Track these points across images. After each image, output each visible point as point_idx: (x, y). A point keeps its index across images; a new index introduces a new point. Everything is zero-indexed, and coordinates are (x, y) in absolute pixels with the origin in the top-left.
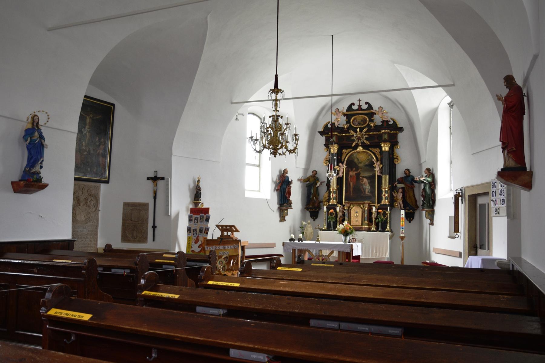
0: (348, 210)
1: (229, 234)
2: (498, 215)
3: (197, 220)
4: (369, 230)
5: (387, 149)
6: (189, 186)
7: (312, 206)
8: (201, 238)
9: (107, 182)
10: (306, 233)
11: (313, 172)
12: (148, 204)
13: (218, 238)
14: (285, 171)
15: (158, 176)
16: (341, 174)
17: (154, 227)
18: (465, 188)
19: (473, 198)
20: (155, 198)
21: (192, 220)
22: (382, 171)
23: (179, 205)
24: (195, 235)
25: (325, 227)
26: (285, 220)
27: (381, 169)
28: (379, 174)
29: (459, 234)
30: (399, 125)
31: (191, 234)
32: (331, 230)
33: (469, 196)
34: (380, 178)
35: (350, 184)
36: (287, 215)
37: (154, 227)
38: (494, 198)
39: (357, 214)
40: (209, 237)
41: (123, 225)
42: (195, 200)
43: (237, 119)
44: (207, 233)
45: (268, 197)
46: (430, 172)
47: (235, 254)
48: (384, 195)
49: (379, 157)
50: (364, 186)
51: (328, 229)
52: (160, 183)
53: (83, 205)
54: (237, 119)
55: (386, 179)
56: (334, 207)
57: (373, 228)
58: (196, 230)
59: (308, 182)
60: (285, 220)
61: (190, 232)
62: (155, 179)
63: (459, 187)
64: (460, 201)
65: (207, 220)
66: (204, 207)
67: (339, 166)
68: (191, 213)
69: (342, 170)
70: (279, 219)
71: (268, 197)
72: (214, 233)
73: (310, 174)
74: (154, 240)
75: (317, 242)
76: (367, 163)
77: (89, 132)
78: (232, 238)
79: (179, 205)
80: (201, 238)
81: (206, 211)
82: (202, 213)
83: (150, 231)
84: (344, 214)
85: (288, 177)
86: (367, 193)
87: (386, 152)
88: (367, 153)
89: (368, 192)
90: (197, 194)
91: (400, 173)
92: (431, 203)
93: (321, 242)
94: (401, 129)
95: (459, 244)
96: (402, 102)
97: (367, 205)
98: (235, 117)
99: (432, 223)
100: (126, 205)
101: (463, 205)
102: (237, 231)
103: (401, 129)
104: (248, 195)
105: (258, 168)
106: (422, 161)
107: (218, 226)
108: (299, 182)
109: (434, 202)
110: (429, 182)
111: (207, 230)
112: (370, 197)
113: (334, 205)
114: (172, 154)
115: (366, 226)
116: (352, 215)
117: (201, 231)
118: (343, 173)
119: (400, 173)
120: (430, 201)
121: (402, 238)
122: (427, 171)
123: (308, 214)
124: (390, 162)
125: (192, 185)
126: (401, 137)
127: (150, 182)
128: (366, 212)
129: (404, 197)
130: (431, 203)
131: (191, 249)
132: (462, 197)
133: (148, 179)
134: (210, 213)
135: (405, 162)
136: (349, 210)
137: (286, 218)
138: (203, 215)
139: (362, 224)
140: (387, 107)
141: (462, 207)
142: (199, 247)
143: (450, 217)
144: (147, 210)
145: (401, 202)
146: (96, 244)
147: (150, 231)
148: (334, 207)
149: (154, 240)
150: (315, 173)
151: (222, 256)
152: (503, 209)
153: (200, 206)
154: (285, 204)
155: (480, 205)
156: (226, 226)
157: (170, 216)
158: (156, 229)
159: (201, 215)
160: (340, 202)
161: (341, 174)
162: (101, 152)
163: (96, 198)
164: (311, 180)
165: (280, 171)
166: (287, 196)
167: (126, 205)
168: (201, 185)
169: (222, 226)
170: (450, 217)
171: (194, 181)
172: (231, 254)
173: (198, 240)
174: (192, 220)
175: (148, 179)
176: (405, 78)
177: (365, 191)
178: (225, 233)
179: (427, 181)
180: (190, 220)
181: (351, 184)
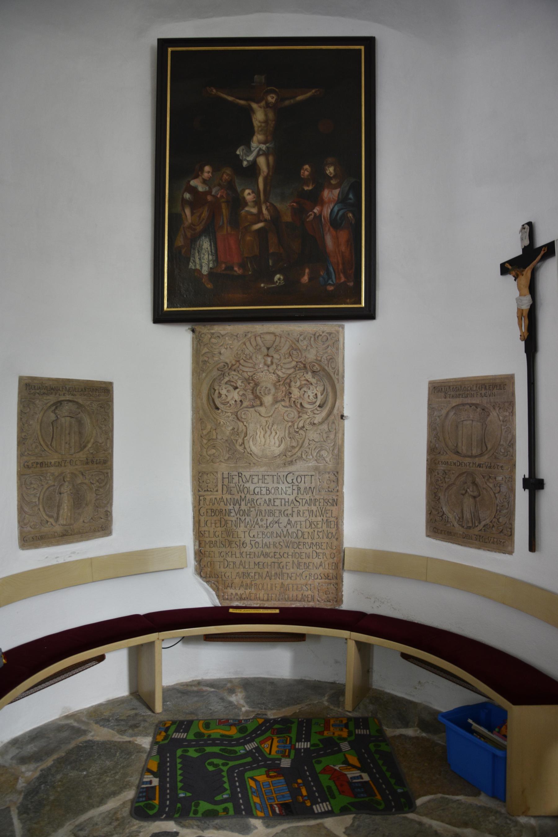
9: (368, 314)
17: (534, 484)
41: (431, 470)
53: (276, 401)
74: (532, 547)
77: (266, 154)
100: (438, 389)
108: (510, 278)
146: (338, 535)
147: (522, 497)
162: (327, 212)
163: (328, 376)
167: (438, 389)
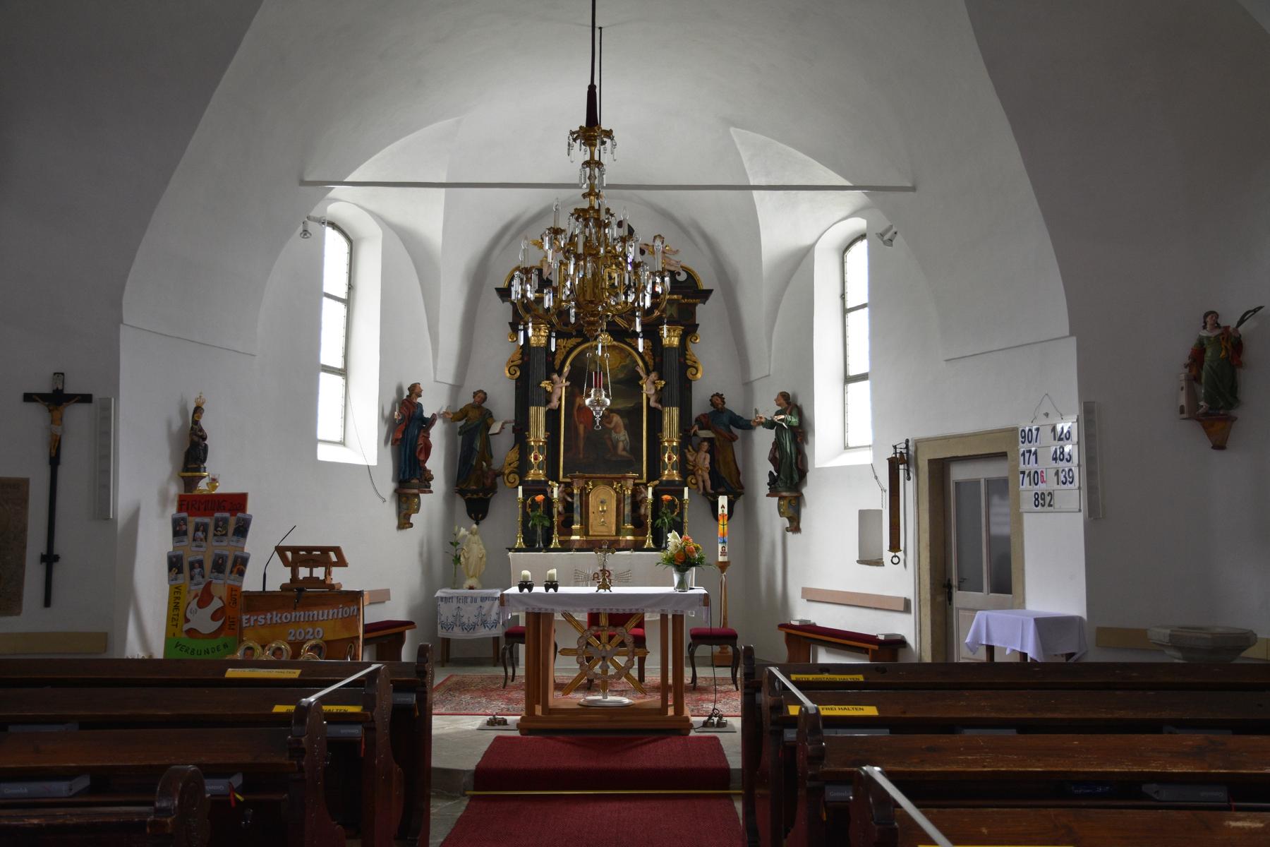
0: (581, 495)
1: (319, 572)
2: (1046, 508)
3: (205, 531)
4: (638, 546)
5: (676, 341)
6: (169, 425)
7: (474, 491)
8: (220, 588)
10: (467, 559)
11: (475, 394)
12: (25, 482)
13: (284, 587)
14: (415, 390)
15: (69, 390)
16: (555, 404)
17: (50, 559)
18: (917, 442)
19: (940, 469)
20: (54, 461)
21: (185, 533)
22: (661, 396)
23: (142, 486)
24: (198, 578)
25: (520, 542)
26: (411, 525)
27: (660, 393)
28: (652, 404)
29: (900, 554)
30: (704, 285)
31: (183, 579)
32: (539, 550)
33: (932, 462)
34: (656, 418)
35: (576, 428)
36: (417, 510)
37: (50, 559)
38: (1032, 467)
39: (603, 506)
40: (251, 583)
42: (186, 469)
43: (305, 232)
44: (241, 573)
45: (373, 461)
46: (789, 403)
47: (346, 635)
48: (670, 458)
49: (651, 362)
50: (614, 435)
51: (530, 546)
52: (76, 415)
54: (305, 232)
55: (671, 416)
56: (541, 487)
57: (649, 542)
58: (201, 563)
59: (462, 423)
60: (411, 525)
61: (180, 571)
62: (56, 399)
63: (900, 441)
64: (901, 472)
65: (242, 530)
66: (218, 491)
67: (553, 382)
68: (180, 510)
69: (558, 391)
70: (395, 522)
71: (373, 461)
72: (265, 573)
73: (467, 399)
74: (47, 603)
75: (602, 591)
76: (621, 376)
78: (332, 587)
79: (142, 486)
80: (220, 588)
81: (237, 502)
82: (224, 510)
83: (33, 574)
84: (569, 507)
85: (420, 406)
86: (620, 451)
87: (671, 348)
88: (622, 350)
89: (624, 449)
90: (193, 451)
91: (699, 406)
92: (796, 477)
93: (616, 590)
94: (705, 295)
95: (900, 578)
96: (710, 227)
97: (630, 483)
98: (300, 229)
99: (795, 526)
101: (910, 485)
102: (342, 562)
103: (705, 295)
104: (325, 454)
105: (339, 380)
106: (756, 373)
107: (281, 550)
109: (803, 474)
110: (791, 427)
111: (241, 563)
112: (632, 462)
113: (539, 482)
114: (121, 321)
115: (629, 538)
116: (591, 509)
117: (219, 566)
118: (560, 399)
119: (699, 406)
120: (791, 473)
121: (723, 566)
122: (782, 401)
123: (461, 505)
124: (676, 370)
125: (177, 423)
126: (703, 312)
127: (37, 415)
128: (628, 501)
129: (713, 462)
130: (796, 477)
131: (187, 627)
132: (907, 463)
133: (28, 397)
134: (250, 509)
135: (711, 377)
136: (584, 494)
137: (414, 518)
138: (227, 515)
139: (618, 532)
140: (673, 239)
141: (908, 489)
142: (214, 617)
143: (863, 515)
144: (24, 501)
145: (707, 476)
148: (541, 487)
149: (47, 603)
150: (481, 396)
151: (302, 643)
152: (1072, 497)
153: (203, 486)
154: (415, 481)
155: (958, 484)
156: (309, 550)
157: (115, 521)
158: (57, 568)
159: (217, 515)
160: (553, 474)
161: (555, 404)
164: (471, 414)
165: (400, 390)
166: (422, 458)
168: (206, 423)
169: (295, 550)
170: (863, 515)
171: (184, 411)
172: (330, 637)
173: (211, 598)
174: (185, 533)
175: (28, 397)
176: (747, 165)
177: (615, 447)
178: (304, 572)
179: (788, 423)
180: (178, 531)
181: (581, 428)
